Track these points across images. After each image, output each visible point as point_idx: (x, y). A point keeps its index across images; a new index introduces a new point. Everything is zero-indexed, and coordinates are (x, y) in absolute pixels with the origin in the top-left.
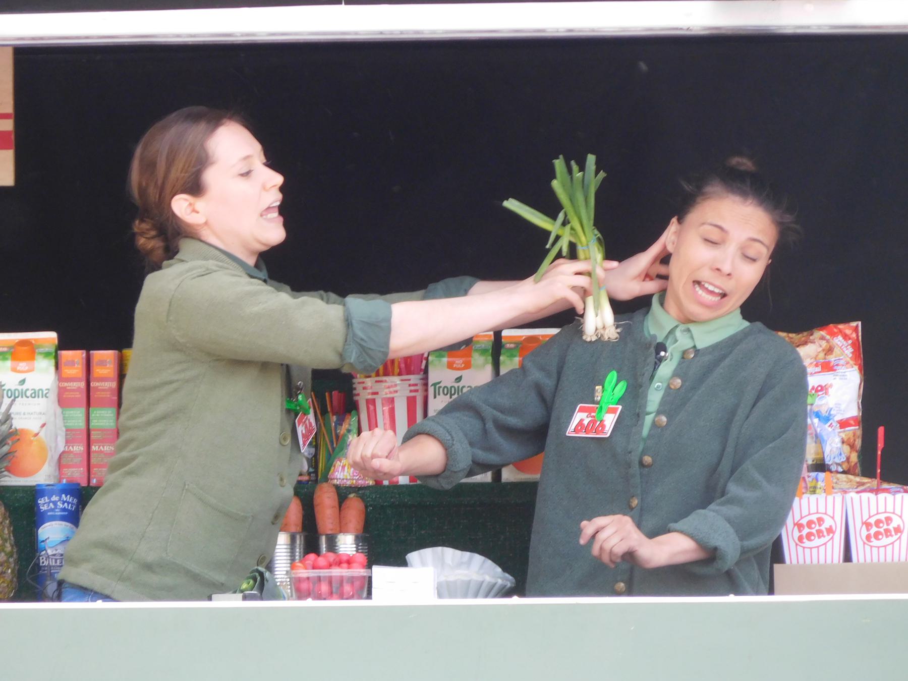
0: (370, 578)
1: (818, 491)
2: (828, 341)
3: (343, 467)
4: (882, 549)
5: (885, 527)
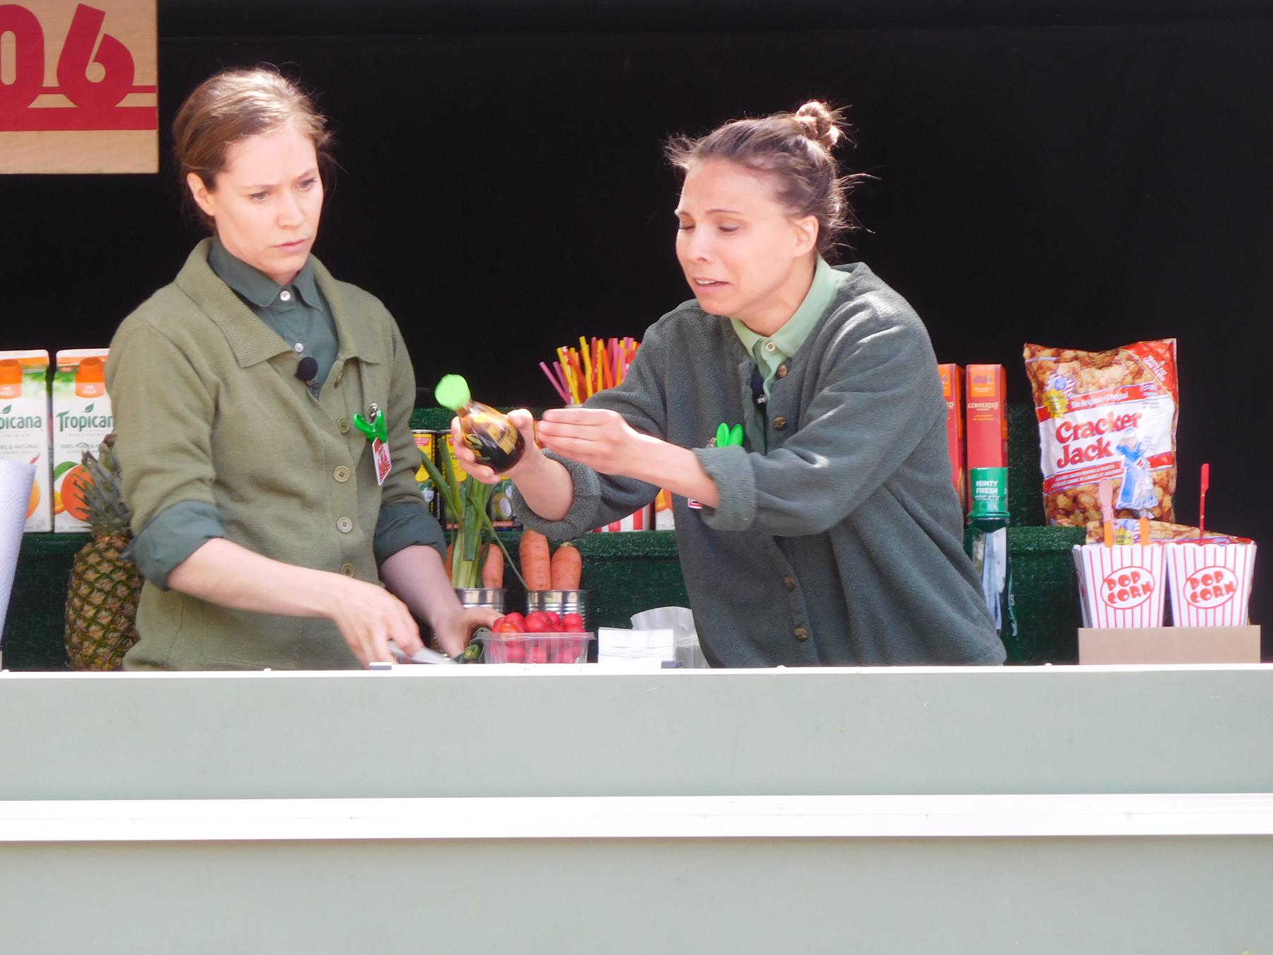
1: (1126, 541)
2: (1136, 362)
5: (1215, 584)
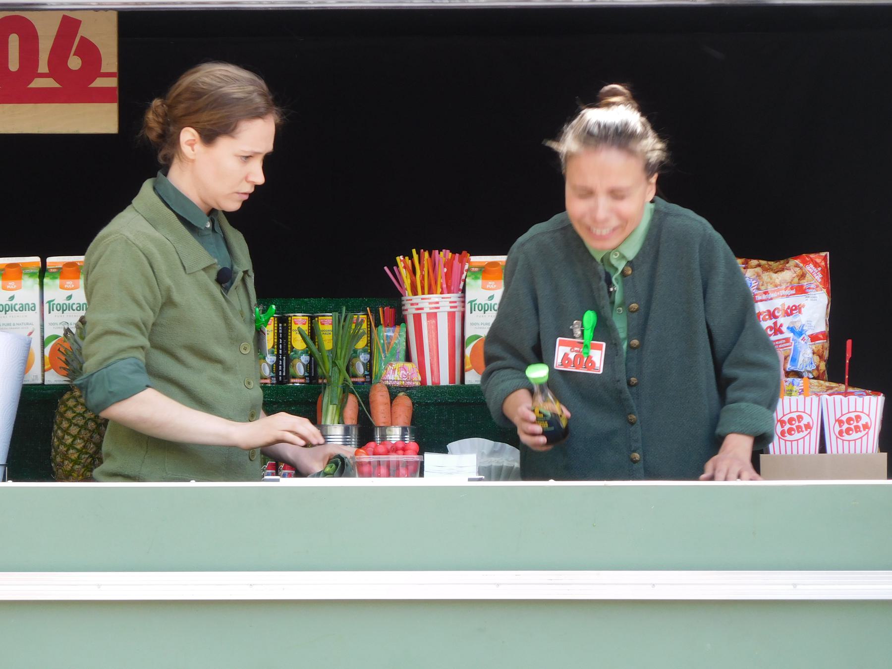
0: (422, 463)
2: (801, 268)
3: (394, 370)
4: (852, 443)
